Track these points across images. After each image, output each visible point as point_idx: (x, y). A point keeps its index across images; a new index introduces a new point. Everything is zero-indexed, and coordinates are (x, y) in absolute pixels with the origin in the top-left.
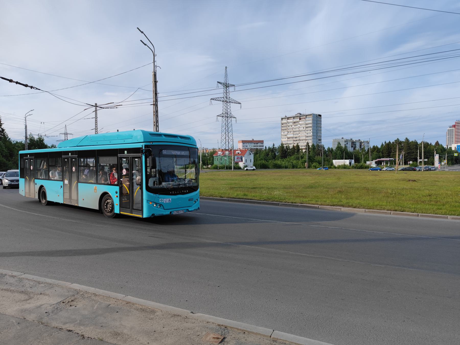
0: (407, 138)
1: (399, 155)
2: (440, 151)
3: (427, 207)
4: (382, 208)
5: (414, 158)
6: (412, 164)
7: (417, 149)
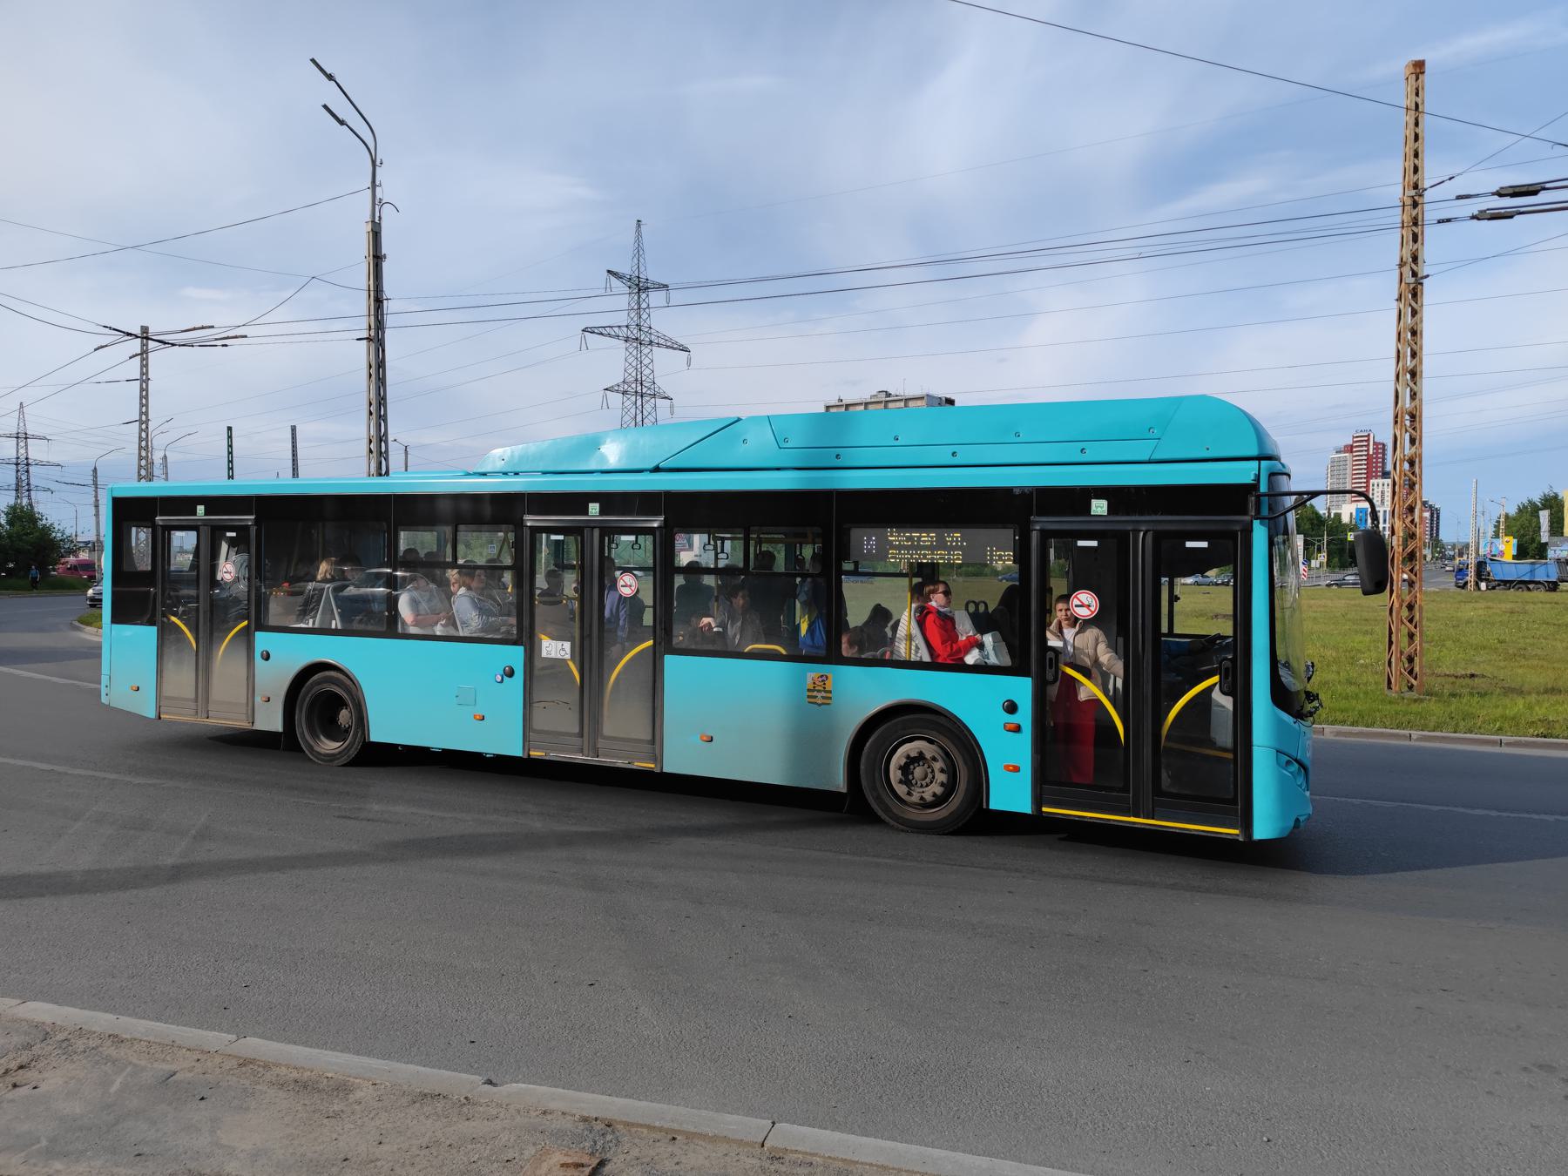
2: (1308, 526)
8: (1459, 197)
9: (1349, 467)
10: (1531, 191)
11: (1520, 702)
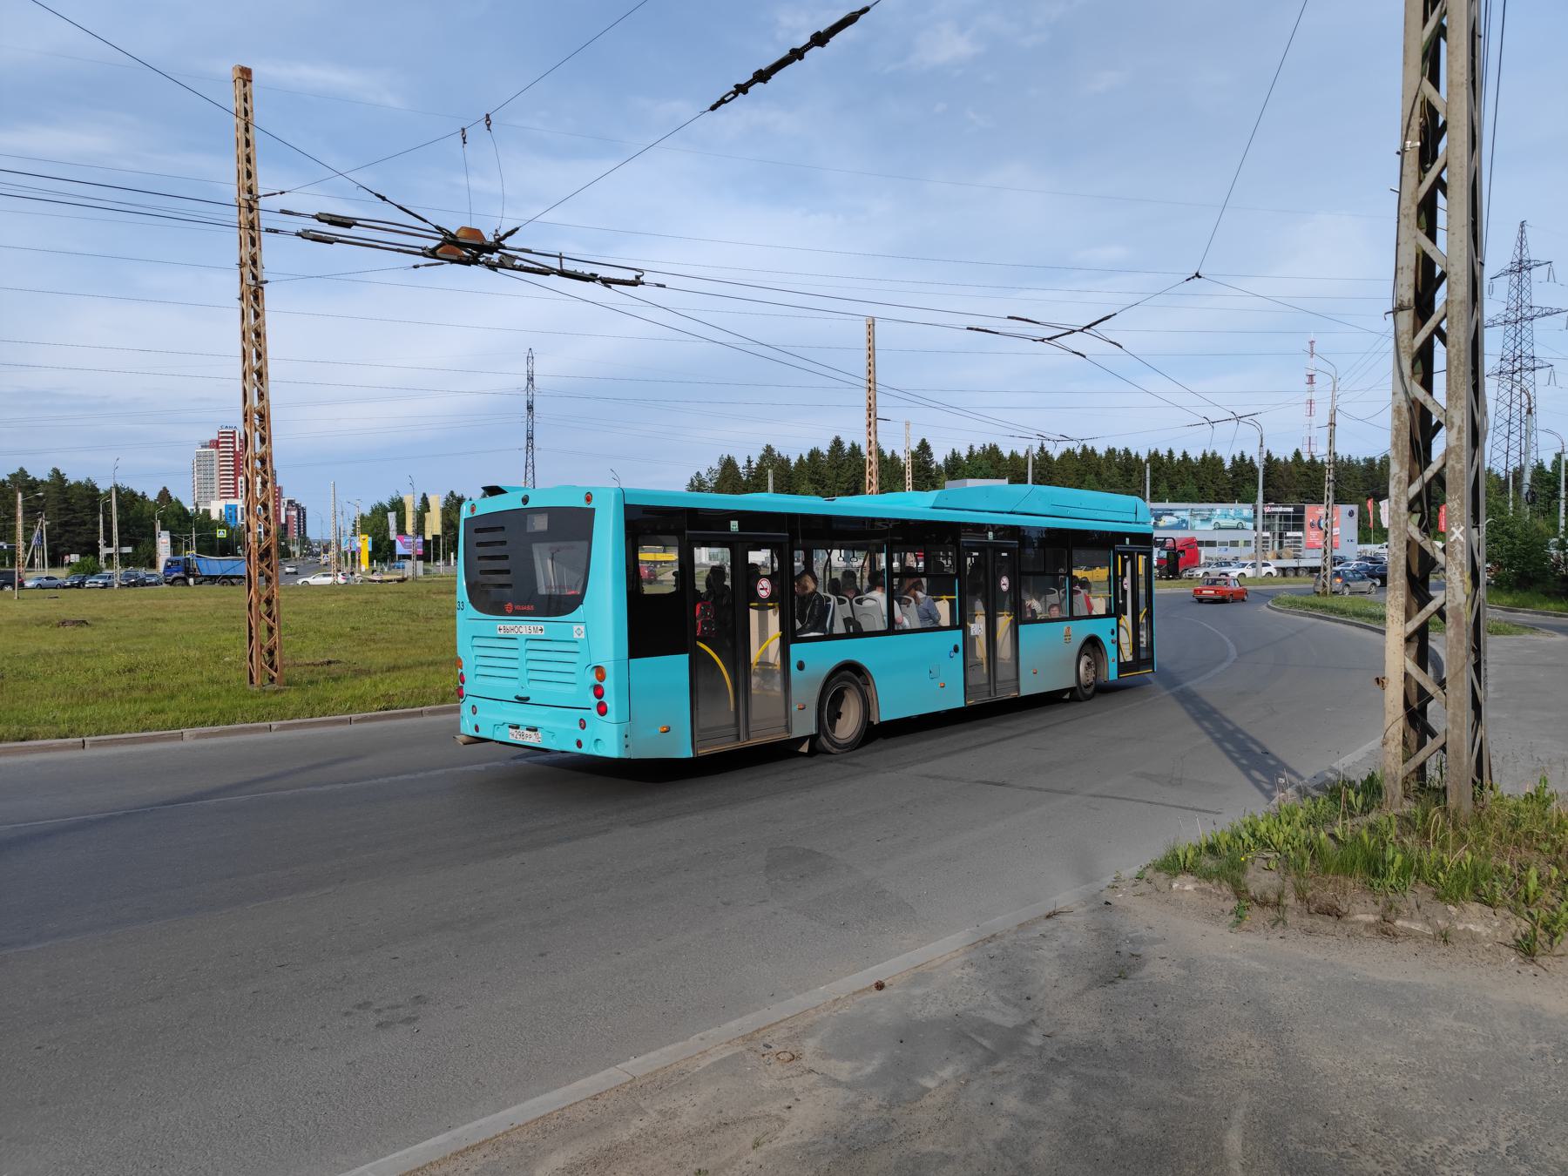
0: (56, 471)
1: (28, 531)
2: (174, 522)
3: (117, 710)
4: (113, 725)
5: (87, 544)
6: (78, 565)
7: (96, 511)
8: (283, 212)
9: (216, 463)
10: (346, 223)
11: (368, 681)
